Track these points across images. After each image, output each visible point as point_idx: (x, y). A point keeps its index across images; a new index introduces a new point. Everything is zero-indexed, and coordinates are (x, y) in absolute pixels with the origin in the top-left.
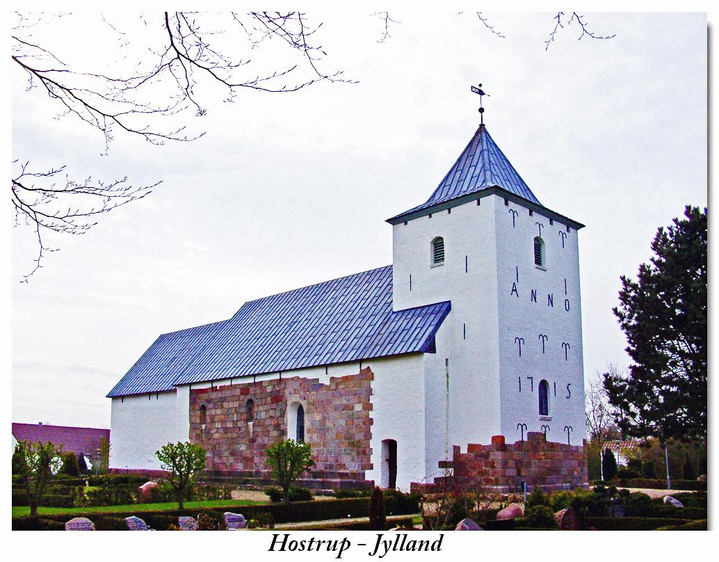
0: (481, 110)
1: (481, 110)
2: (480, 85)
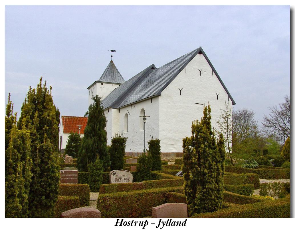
0: (112, 56)
1: (112, 56)
2: (112, 49)
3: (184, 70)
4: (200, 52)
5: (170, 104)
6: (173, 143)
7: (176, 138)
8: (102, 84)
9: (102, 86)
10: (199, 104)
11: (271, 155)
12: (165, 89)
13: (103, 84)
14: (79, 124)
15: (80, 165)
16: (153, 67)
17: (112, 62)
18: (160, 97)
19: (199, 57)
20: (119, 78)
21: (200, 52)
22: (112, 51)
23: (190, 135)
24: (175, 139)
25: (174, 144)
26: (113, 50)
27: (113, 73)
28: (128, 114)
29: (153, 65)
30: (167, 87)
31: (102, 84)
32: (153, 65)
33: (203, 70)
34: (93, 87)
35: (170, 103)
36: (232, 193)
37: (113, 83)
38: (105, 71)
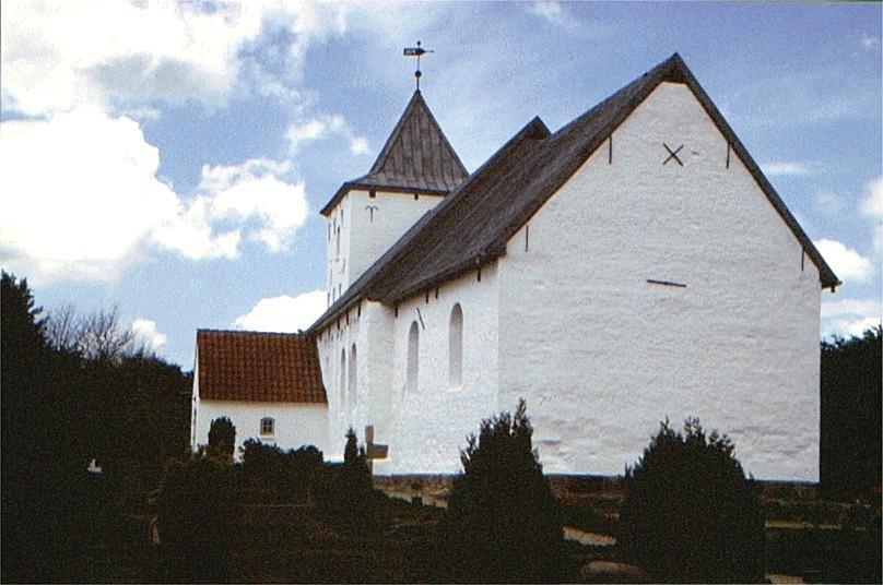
1: (418, 74)
2: (419, 43)
3: (602, 151)
4: (674, 71)
5: (542, 287)
6: (556, 437)
7: (568, 420)
8: (372, 195)
10: (666, 283)
12: (524, 228)
14: (809, 566)
16: (536, 130)
18: (501, 263)
19: (667, 88)
21: (674, 71)
24: (563, 422)
25: (559, 442)
28: (419, 322)
30: (529, 223)
31: (372, 195)
34: (338, 207)
35: (541, 283)
36: (603, 563)
37: (417, 192)
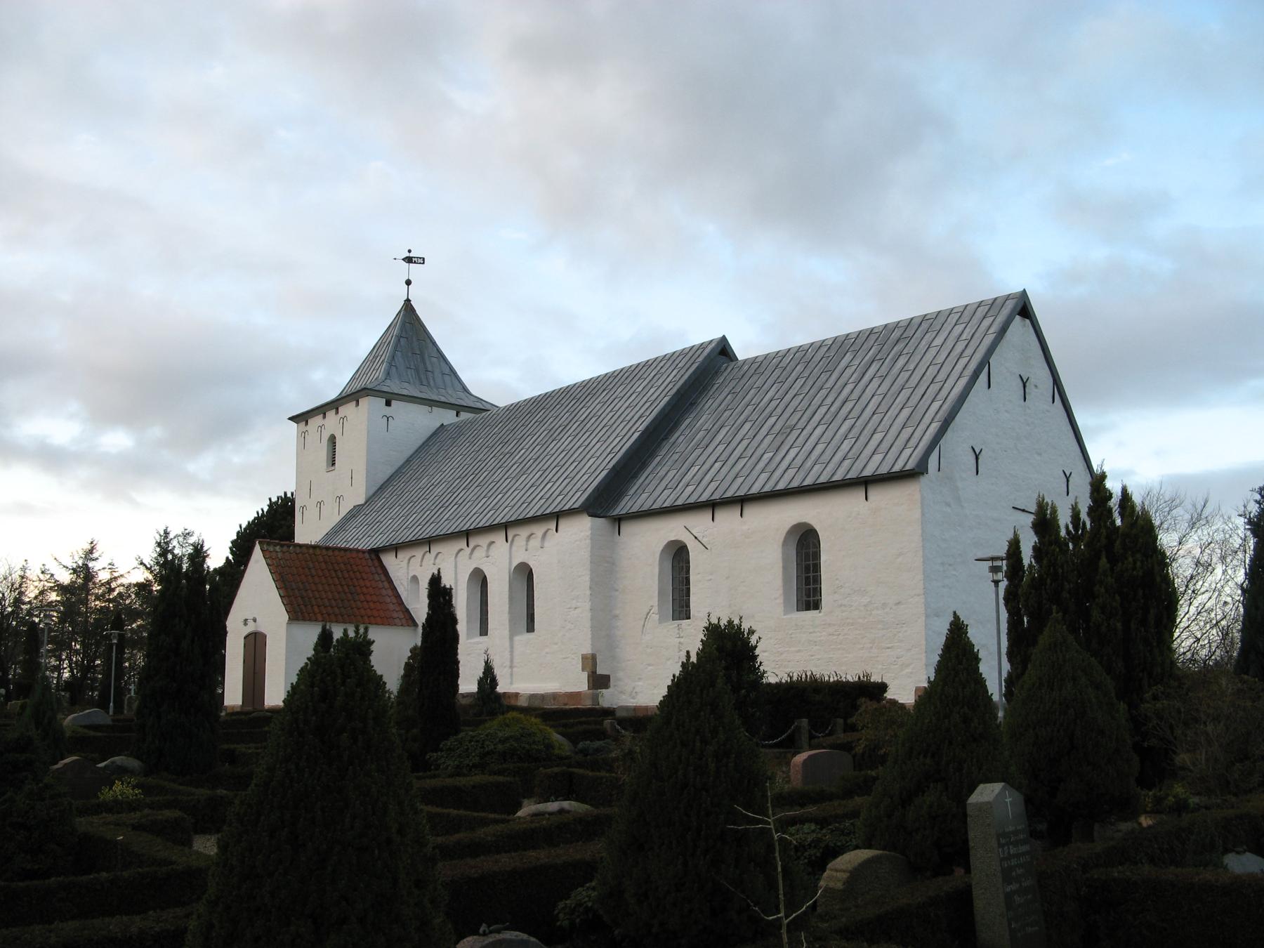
0: (408, 283)
1: (408, 283)
2: (410, 251)
3: (983, 377)
8: (388, 404)
9: (388, 411)
10: (1023, 511)
11: (541, 727)
13: (393, 402)
15: (813, 858)
17: (408, 307)
20: (447, 378)
22: (409, 260)
23: (410, 654)
26: (411, 255)
27: (422, 355)
29: (724, 339)
31: (388, 404)
32: (724, 339)
33: (1032, 380)
37: (431, 403)
38: (377, 343)
